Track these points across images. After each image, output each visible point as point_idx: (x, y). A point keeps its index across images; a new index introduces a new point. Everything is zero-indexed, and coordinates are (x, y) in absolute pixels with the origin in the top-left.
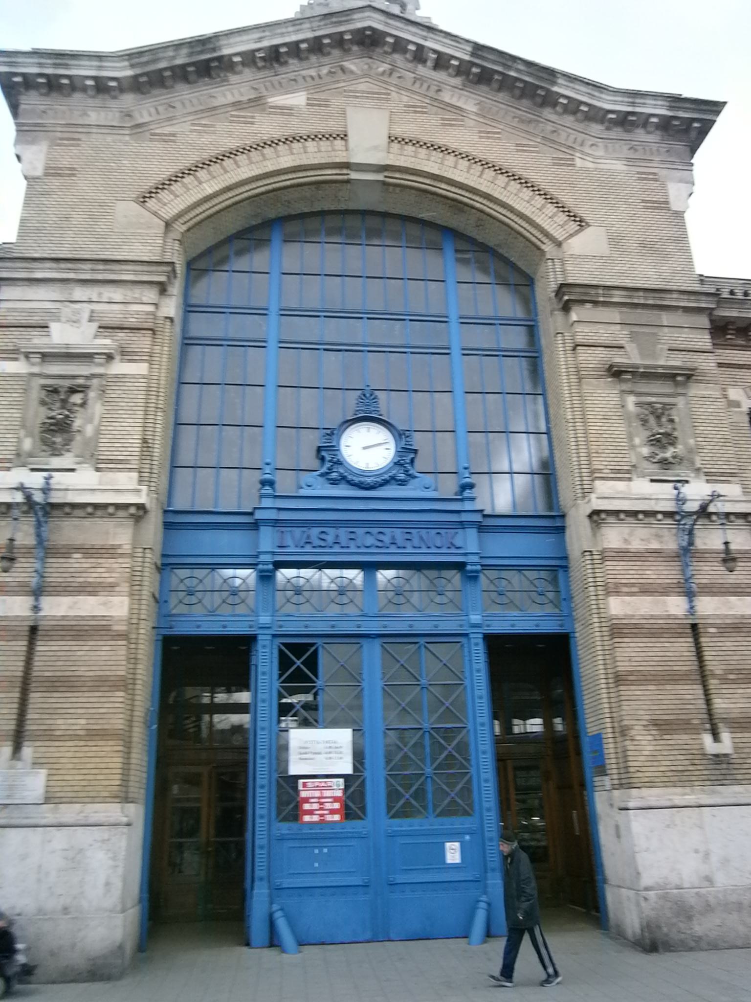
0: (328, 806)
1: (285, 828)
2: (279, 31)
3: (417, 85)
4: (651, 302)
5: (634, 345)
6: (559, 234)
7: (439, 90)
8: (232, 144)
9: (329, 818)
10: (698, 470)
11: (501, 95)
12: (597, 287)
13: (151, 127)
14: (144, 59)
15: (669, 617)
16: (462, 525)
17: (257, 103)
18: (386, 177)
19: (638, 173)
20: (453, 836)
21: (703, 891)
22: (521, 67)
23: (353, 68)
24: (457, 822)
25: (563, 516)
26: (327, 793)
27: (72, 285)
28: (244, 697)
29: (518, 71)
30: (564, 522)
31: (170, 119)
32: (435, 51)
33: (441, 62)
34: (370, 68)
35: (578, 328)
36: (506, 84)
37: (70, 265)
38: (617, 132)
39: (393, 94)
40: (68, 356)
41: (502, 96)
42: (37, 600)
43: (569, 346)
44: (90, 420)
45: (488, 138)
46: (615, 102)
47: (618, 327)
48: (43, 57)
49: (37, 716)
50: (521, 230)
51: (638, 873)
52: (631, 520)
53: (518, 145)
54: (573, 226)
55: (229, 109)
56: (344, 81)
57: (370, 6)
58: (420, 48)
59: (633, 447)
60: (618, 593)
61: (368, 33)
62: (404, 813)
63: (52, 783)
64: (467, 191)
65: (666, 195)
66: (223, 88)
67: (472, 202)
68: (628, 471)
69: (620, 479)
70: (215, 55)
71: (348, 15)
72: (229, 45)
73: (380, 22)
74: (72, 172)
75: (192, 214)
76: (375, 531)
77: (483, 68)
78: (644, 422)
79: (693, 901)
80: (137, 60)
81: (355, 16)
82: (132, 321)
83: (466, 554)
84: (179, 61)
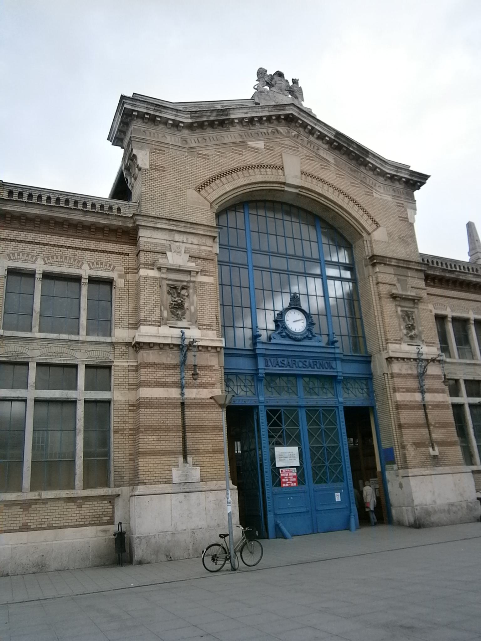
0: (291, 480)
1: (276, 489)
2: (255, 110)
3: (309, 145)
4: (405, 266)
5: (399, 284)
6: (369, 229)
7: (318, 149)
8: (235, 165)
9: (292, 485)
10: (423, 341)
11: (344, 156)
12: (386, 257)
13: (197, 150)
14: (197, 115)
15: (416, 401)
16: (335, 359)
17: (243, 144)
18: (299, 191)
19: (397, 203)
20: (338, 490)
21: (433, 506)
22: (355, 147)
23: (282, 131)
24: (339, 485)
25: (370, 356)
26: (291, 474)
27: (173, 233)
28: (222, 433)
29: (353, 148)
30: (371, 358)
31: (206, 146)
32: (319, 131)
33: (321, 137)
34: (289, 132)
35: (379, 275)
36: (348, 153)
37: (174, 223)
38: (388, 182)
39: (300, 148)
40: (179, 271)
41: (344, 157)
42: (182, 390)
43: (375, 282)
44: (192, 304)
45: (340, 177)
46: (390, 170)
47: (393, 276)
48: (149, 105)
49: (191, 444)
50: (354, 225)
51: (413, 500)
52: (402, 361)
53: (351, 183)
54: (374, 226)
55: (231, 145)
56: (279, 138)
57: (293, 104)
58: (313, 128)
59: (401, 330)
60: (399, 391)
61: (291, 116)
62: (320, 481)
63: (202, 473)
64: (332, 202)
65: (407, 214)
66: (227, 133)
67: (334, 208)
68: (399, 340)
69: (397, 343)
70: (227, 117)
71: (284, 107)
72: (234, 114)
73: (296, 112)
74: (163, 169)
75: (220, 200)
76: (303, 360)
77: (339, 143)
78: (404, 319)
79: (430, 509)
80: (193, 115)
81: (287, 108)
82: (203, 255)
83: (337, 372)
84: (212, 118)
